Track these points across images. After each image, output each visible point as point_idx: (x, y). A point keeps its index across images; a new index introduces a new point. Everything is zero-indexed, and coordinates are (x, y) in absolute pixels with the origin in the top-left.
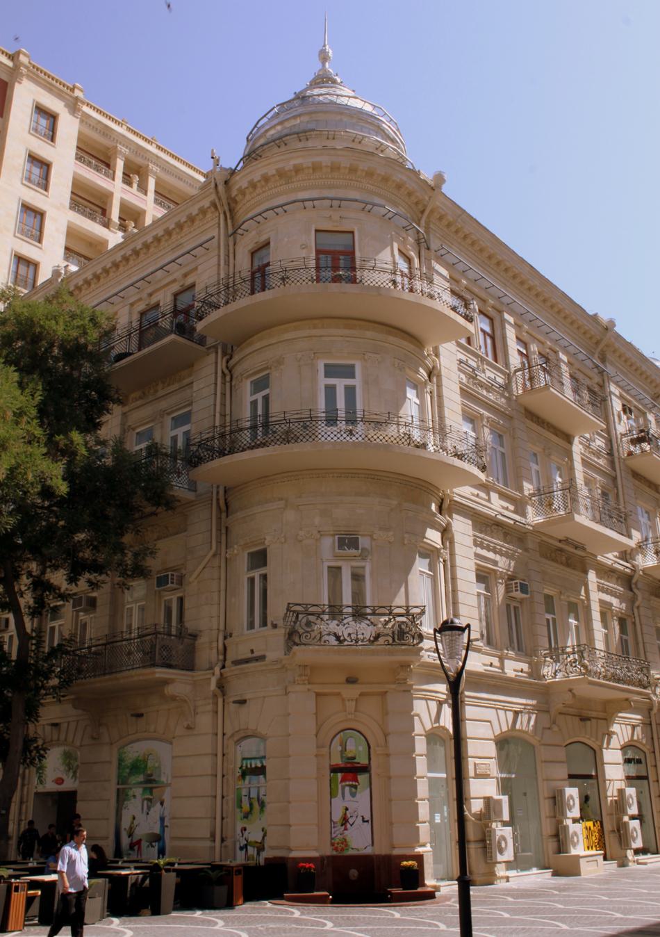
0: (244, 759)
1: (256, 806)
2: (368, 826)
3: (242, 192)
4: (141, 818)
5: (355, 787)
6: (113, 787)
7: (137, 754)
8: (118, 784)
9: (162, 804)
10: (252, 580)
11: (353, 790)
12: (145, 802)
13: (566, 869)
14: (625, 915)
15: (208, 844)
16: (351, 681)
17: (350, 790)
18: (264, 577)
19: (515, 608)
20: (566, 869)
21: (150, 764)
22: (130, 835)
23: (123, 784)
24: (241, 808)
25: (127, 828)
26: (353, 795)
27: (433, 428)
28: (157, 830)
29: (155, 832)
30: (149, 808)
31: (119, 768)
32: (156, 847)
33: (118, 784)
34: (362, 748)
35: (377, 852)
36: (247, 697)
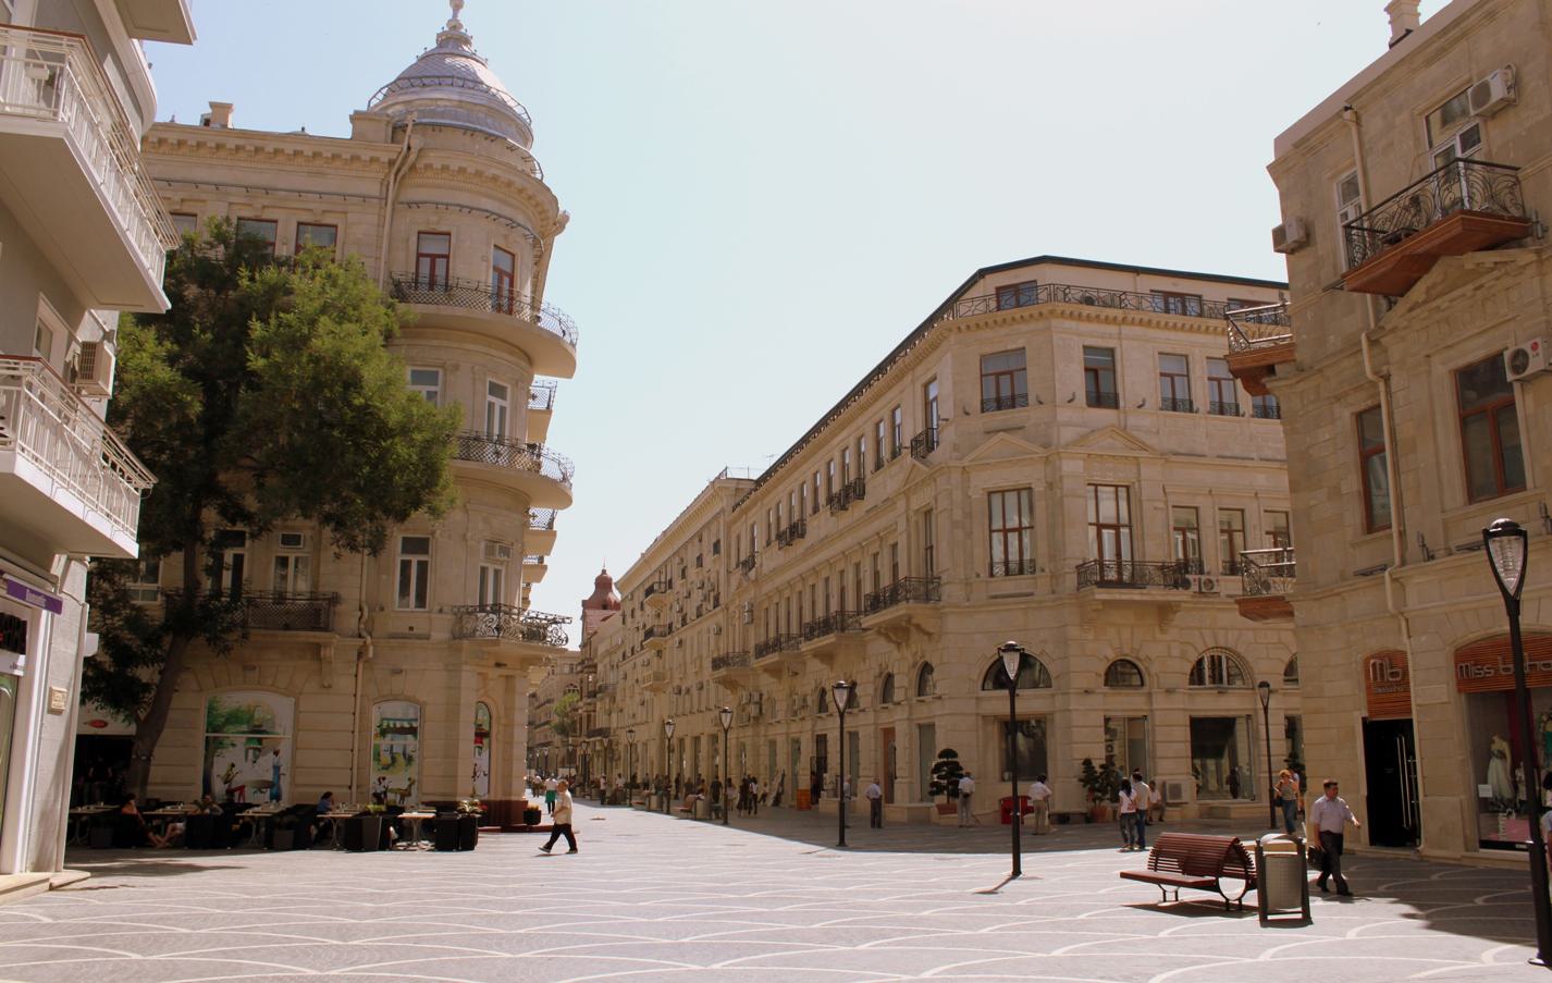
0: (383, 719)
1: (401, 759)
2: (486, 778)
3: (428, 167)
4: (241, 765)
5: (481, 748)
6: (201, 735)
7: (237, 705)
8: (207, 731)
9: (276, 753)
10: (406, 565)
11: (257, 753)
12: (251, 752)
13: (940, 756)
14: (345, 941)
15: (346, 790)
16: (498, 665)
17: (254, 754)
18: (423, 566)
19: (497, 572)
20: (940, 756)
21: (256, 716)
22: (227, 781)
23: (214, 732)
24: (379, 760)
25: (223, 774)
26: (480, 754)
27: (906, 699)
28: (269, 777)
29: (265, 778)
30: (256, 757)
31: (208, 717)
32: (268, 793)
33: (207, 731)
34: (486, 718)
35: (492, 798)
36: (404, 667)
